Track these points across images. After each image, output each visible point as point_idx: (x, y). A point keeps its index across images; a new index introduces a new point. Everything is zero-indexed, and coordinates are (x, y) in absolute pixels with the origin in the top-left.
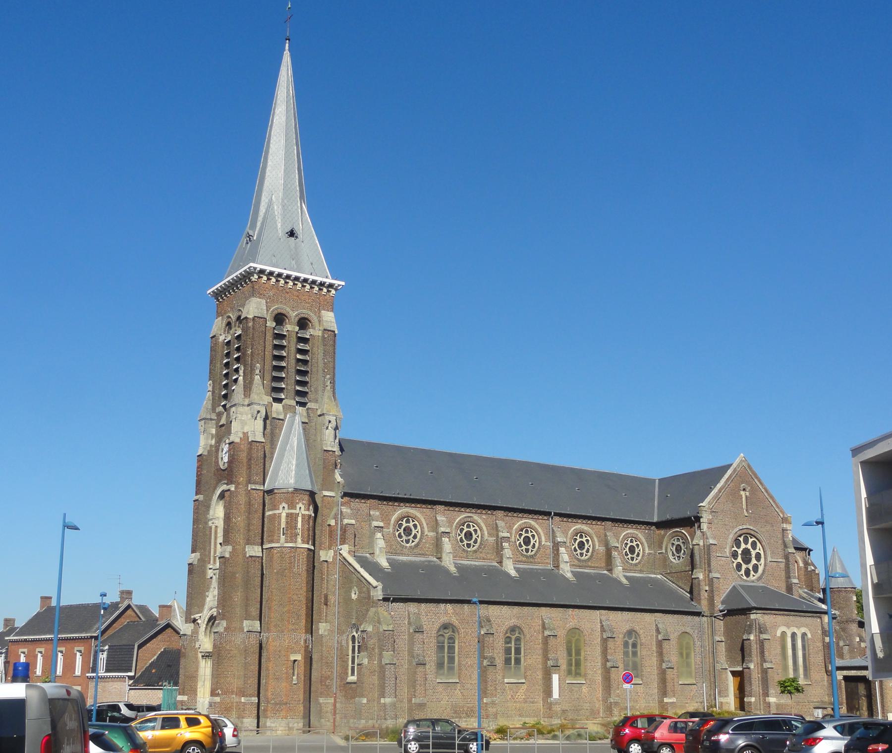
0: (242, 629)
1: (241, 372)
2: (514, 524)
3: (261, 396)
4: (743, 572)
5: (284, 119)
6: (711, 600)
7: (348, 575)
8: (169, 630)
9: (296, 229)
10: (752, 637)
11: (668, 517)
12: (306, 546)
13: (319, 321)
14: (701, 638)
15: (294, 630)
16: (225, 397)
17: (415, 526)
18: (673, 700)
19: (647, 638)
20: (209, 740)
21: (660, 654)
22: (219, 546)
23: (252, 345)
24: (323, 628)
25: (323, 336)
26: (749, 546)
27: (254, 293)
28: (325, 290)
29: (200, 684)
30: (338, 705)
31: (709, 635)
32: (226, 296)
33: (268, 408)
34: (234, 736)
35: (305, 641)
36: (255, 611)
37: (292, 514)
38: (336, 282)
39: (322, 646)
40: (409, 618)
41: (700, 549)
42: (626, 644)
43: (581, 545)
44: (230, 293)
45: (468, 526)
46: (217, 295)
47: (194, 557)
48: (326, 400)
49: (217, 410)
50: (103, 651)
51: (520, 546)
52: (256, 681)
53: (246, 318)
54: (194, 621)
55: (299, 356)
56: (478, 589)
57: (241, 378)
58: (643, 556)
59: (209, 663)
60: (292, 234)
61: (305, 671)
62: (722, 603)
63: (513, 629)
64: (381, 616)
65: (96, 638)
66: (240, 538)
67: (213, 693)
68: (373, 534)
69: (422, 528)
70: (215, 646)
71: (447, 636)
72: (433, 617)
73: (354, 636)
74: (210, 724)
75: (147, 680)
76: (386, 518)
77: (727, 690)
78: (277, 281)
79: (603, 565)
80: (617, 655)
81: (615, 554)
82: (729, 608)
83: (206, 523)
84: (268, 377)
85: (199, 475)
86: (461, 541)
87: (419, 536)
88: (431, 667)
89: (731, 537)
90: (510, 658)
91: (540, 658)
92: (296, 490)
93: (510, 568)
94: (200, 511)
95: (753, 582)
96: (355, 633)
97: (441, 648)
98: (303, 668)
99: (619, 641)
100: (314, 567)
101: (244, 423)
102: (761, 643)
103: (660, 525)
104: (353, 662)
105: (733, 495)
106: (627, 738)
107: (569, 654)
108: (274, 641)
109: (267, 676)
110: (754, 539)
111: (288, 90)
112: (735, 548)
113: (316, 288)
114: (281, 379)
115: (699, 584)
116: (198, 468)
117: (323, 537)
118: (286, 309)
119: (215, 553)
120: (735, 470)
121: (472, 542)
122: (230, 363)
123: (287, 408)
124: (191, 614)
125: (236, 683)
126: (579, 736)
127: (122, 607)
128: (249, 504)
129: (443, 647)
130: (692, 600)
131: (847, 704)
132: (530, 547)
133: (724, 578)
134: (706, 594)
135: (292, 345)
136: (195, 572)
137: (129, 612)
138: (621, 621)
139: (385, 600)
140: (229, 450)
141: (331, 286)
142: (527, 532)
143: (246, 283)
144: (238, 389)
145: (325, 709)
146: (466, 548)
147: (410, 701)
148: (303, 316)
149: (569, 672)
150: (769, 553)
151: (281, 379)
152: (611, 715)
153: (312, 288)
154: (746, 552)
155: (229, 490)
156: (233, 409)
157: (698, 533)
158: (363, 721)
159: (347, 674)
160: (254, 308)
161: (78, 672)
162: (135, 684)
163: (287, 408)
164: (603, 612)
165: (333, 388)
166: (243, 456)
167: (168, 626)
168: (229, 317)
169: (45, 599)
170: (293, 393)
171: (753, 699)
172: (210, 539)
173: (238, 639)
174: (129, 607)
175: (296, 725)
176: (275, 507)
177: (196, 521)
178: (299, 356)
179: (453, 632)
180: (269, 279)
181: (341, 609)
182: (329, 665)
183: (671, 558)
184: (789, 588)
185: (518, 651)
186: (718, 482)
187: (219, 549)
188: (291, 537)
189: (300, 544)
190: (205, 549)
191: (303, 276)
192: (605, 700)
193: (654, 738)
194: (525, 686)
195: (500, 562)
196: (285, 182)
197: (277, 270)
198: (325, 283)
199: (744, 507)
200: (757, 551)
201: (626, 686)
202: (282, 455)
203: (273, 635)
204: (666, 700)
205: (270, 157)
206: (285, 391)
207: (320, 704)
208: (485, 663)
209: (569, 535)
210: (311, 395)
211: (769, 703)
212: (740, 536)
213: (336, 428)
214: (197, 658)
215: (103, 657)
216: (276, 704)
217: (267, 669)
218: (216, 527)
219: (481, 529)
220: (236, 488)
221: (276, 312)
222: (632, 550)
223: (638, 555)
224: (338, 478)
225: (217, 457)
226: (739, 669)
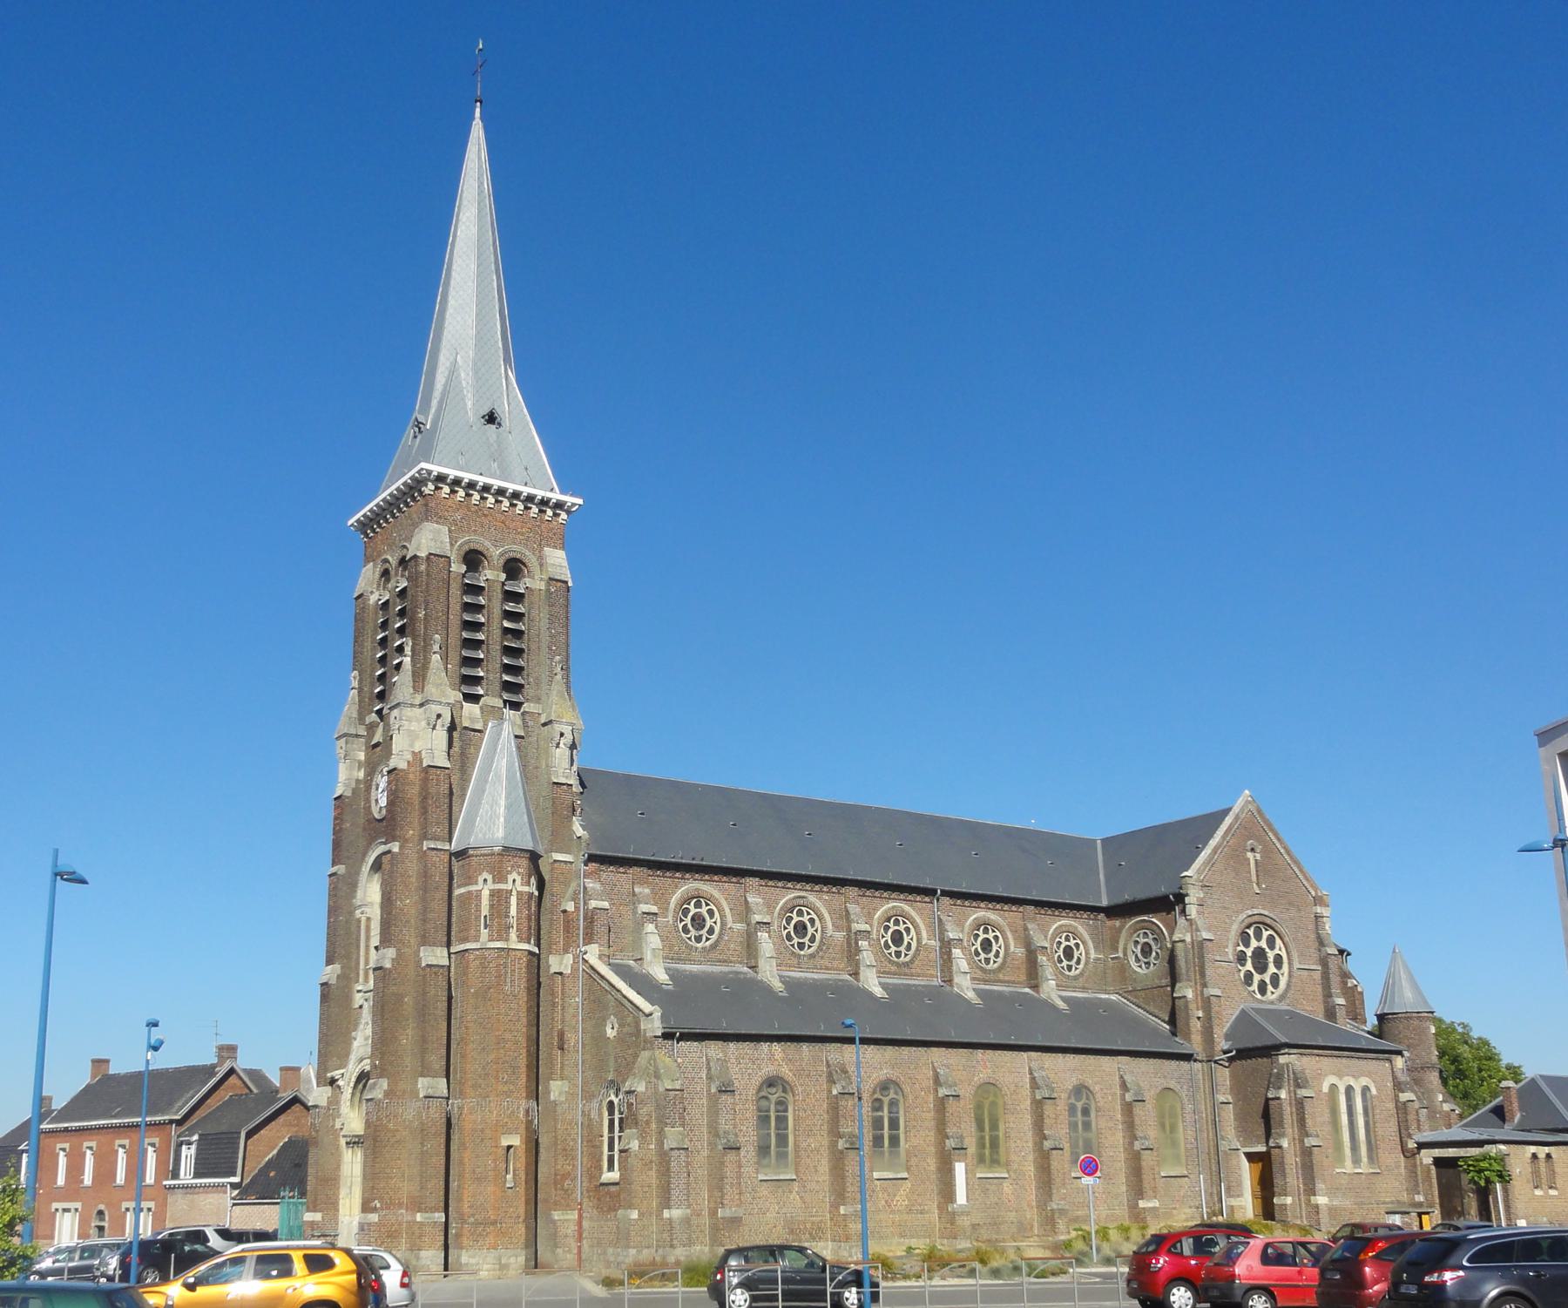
0: (415, 1093)
1: (408, 650)
2: (876, 910)
3: (443, 689)
4: (1255, 987)
5: (474, 230)
6: (1208, 1033)
7: (599, 996)
8: (297, 1108)
9: (498, 411)
10: (1283, 1094)
11: (1127, 897)
12: (525, 946)
13: (541, 565)
14: (1193, 1098)
15: (508, 1094)
16: (381, 696)
17: (711, 913)
18: (1154, 1203)
19: (1107, 1099)
20: (352, 1299)
21: (1130, 1125)
22: (373, 951)
23: (427, 604)
24: (556, 1089)
25: (548, 590)
26: (1263, 944)
27: (427, 515)
28: (550, 512)
29: (343, 1192)
30: (585, 1224)
31: (1203, 1095)
32: (380, 526)
33: (455, 708)
34: (403, 1285)
35: (527, 1111)
36: (437, 1062)
37: (499, 891)
38: (569, 499)
39: (555, 1120)
40: (709, 1069)
41: (1186, 950)
42: (1072, 1109)
43: (987, 945)
44: (387, 521)
45: (800, 913)
46: (365, 526)
47: (331, 973)
48: (554, 697)
51: (887, 946)
52: (442, 1183)
53: (415, 557)
54: (333, 1082)
55: (506, 624)
56: (818, 1020)
57: (407, 660)
59: (359, 1154)
60: (491, 418)
61: (527, 1164)
62: (1227, 1037)
63: (884, 1086)
64: (661, 1065)
65: (179, 1123)
66: (410, 935)
67: (366, 1208)
68: (639, 926)
69: (722, 917)
70: (368, 1124)
71: (773, 1098)
72: (749, 1065)
73: (611, 1103)
74: (353, 1266)
75: (259, 1189)
76: (661, 898)
77: (1240, 1184)
78: (468, 495)
79: (1023, 978)
80: (1059, 1129)
81: (1042, 959)
82: (1241, 1046)
83: (351, 913)
84: (454, 659)
85: (337, 832)
86: (789, 938)
87: (717, 929)
88: (749, 1153)
89: (1235, 929)
90: (882, 1137)
91: (931, 1136)
92: (506, 849)
93: (872, 983)
94: (341, 894)
95: (1272, 1003)
96: (613, 1097)
97: (764, 1120)
98: (523, 1159)
99: (1062, 1106)
100: (539, 984)
101: (413, 736)
102: (1300, 1104)
103: (1113, 912)
104: (611, 1148)
105: (1236, 857)
106: (1162, 1278)
107: (981, 1128)
108: (472, 1113)
109: (461, 1176)
110: (1271, 932)
111: (481, 184)
112: (1242, 948)
113: (535, 509)
114: (476, 662)
115: (1186, 1006)
117: (554, 931)
119: (367, 962)
120: (1237, 818)
121: (806, 940)
122: (385, 641)
123: (489, 712)
124: (327, 1070)
125: (407, 1189)
126: (1016, 1269)
127: (221, 1071)
128: (425, 875)
129: (768, 1117)
130: (1174, 1034)
131: (1441, 1206)
132: (902, 949)
133: (1226, 997)
134: (1199, 1024)
135: (494, 604)
136: (332, 998)
137: (233, 1080)
138: (1063, 1071)
139: (667, 1036)
140: (389, 783)
141: (559, 505)
142: (897, 923)
143: (414, 499)
144: (402, 683)
145: (562, 1231)
146: (797, 950)
147: (713, 1213)
148: (512, 555)
149: (981, 1159)
150: (1295, 955)
151: (476, 662)
152: (1054, 1231)
153: (527, 508)
154: (1259, 955)
155: (389, 852)
156: (395, 713)
157: (1181, 921)
158: (633, 1251)
159: (601, 1169)
160: (429, 539)
161: (150, 1178)
162: (242, 1196)
163: (489, 712)
164: (1033, 1054)
165: (567, 678)
166: (413, 792)
167: (295, 1100)
168: (386, 561)
169: (99, 1063)
170: (497, 686)
171: (1289, 1200)
172: (358, 940)
173: (409, 1112)
174: (232, 1071)
175: (512, 1260)
176: (470, 880)
177: (333, 911)
178: (506, 624)
179: (784, 1091)
180: (453, 492)
181: (587, 1057)
182: (568, 1154)
184: (1331, 1013)
185: (894, 1124)
186: (1211, 836)
187: (373, 954)
189: (514, 943)
190: (348, 956)
191: (511, 487)
192: (1042, 1204)
193: (1233, 1276)
194: (908, 1184)
195: (856, 974)
196: (478, 333)
197: (467, 477)
198: (549, 500)
199: (1254, 878)
200: (1277, 951)
201: (1087, 1180)
202: (480, 791)
203: (470, 1102)
204: (1142, 1204)
205: (452, 293)
206: (484, 682)
207: (554, 1222)
208: (841, 1144)
209: (966, 929)
210: (529, 691)
211: (1317, 1206)
212: (1248, 927)
213: (573, 747)
214: (338, 1147)
215: (188, 1154)
217: (461, 1163)
218: (368, 919)
219: (821, 918)
221: (466, 548)
222: (1068, 953)
223: (1078, 962)
224: (578, 829)
225: (368, 800)
226: (1262, 1148)
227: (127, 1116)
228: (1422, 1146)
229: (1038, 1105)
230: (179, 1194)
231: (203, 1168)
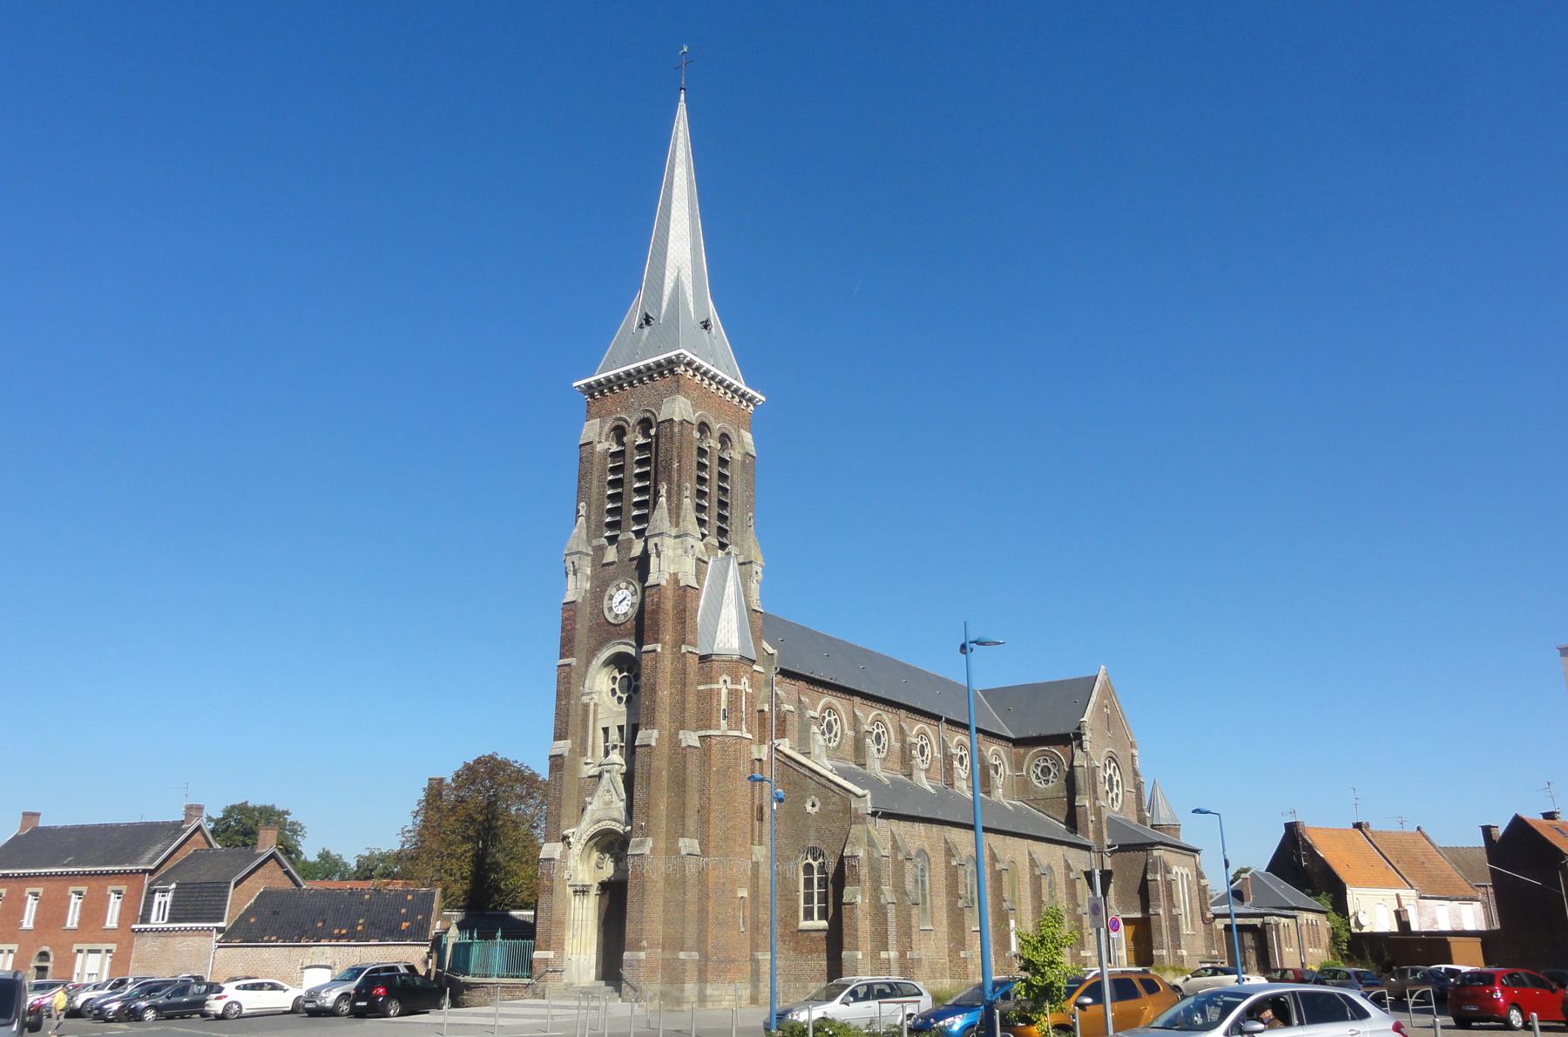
25: (743, 462)
49: (595, 543)
50: (166, 891)
54: (565, 838)
65: (151, 872)
103: (1017, 743)
118: (711, 420)
137: (198, 836)
139: (874, 814)
169: (30, 816)
176: (711, 680)
195: (910, 775)
204: (1083, 953)
227: (76, 864)
228: (1216, 916)
229: (1036, 880)
230: (149, 938)
231: (178, 913)
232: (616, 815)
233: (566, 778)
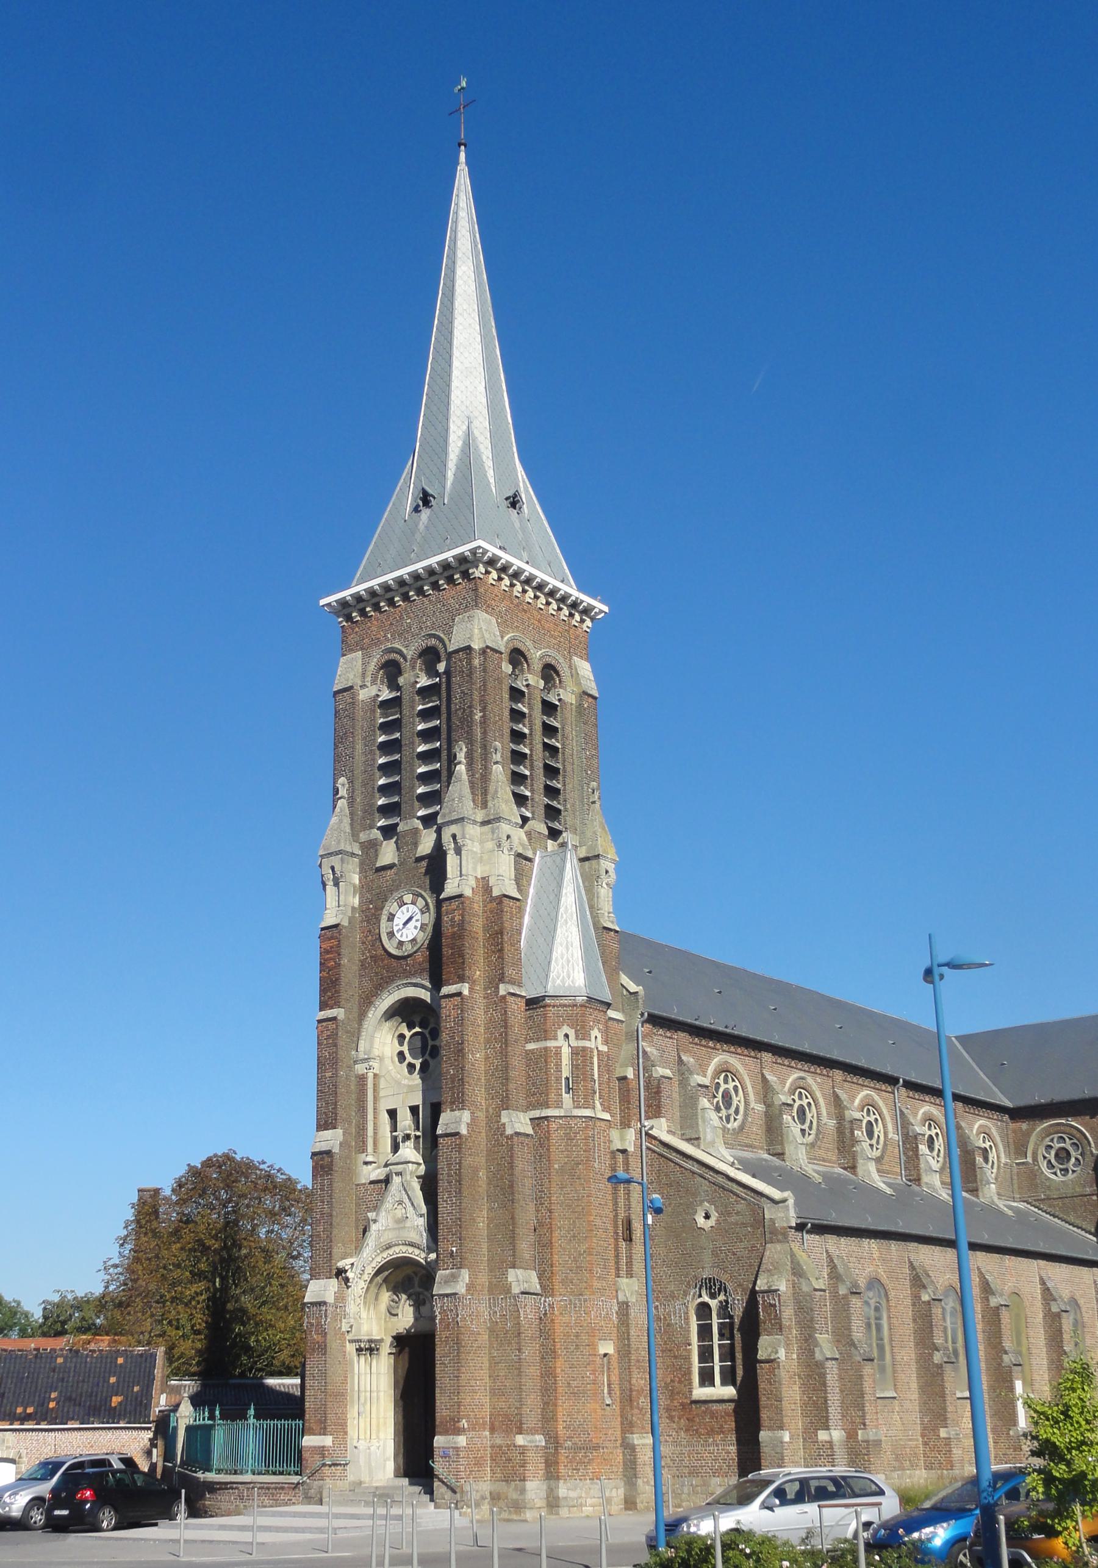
25: (580, 706)
30: (664, 1450)
37: (584, 1049)
58: (999, 1167)
103: (1016, 1114)
116: (324, 952)
139: (800, 1227)
159: (691, 1384)
180: (500, 579)
183: (1047, 1172)
188: (585, 1097)
195: (853, 1168)
216: (577, 1448)
220: (471, 990)
232: (414, 1237)
233: (338, 1185)
